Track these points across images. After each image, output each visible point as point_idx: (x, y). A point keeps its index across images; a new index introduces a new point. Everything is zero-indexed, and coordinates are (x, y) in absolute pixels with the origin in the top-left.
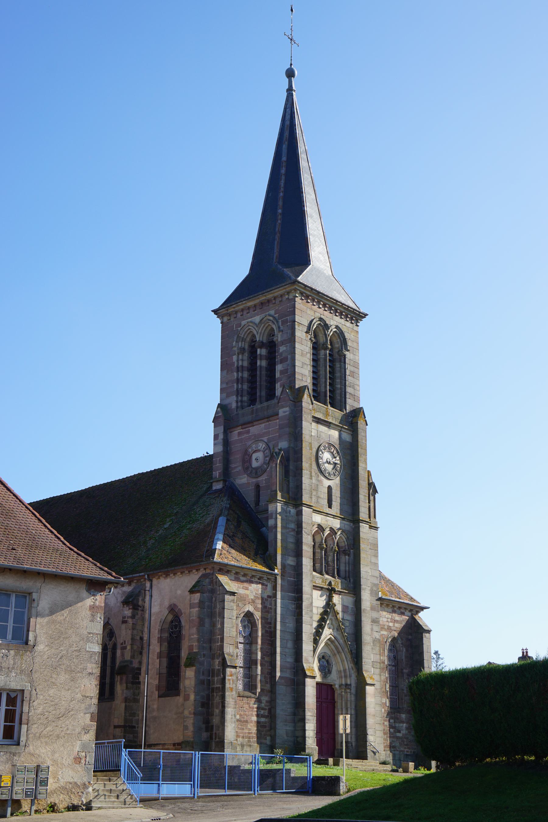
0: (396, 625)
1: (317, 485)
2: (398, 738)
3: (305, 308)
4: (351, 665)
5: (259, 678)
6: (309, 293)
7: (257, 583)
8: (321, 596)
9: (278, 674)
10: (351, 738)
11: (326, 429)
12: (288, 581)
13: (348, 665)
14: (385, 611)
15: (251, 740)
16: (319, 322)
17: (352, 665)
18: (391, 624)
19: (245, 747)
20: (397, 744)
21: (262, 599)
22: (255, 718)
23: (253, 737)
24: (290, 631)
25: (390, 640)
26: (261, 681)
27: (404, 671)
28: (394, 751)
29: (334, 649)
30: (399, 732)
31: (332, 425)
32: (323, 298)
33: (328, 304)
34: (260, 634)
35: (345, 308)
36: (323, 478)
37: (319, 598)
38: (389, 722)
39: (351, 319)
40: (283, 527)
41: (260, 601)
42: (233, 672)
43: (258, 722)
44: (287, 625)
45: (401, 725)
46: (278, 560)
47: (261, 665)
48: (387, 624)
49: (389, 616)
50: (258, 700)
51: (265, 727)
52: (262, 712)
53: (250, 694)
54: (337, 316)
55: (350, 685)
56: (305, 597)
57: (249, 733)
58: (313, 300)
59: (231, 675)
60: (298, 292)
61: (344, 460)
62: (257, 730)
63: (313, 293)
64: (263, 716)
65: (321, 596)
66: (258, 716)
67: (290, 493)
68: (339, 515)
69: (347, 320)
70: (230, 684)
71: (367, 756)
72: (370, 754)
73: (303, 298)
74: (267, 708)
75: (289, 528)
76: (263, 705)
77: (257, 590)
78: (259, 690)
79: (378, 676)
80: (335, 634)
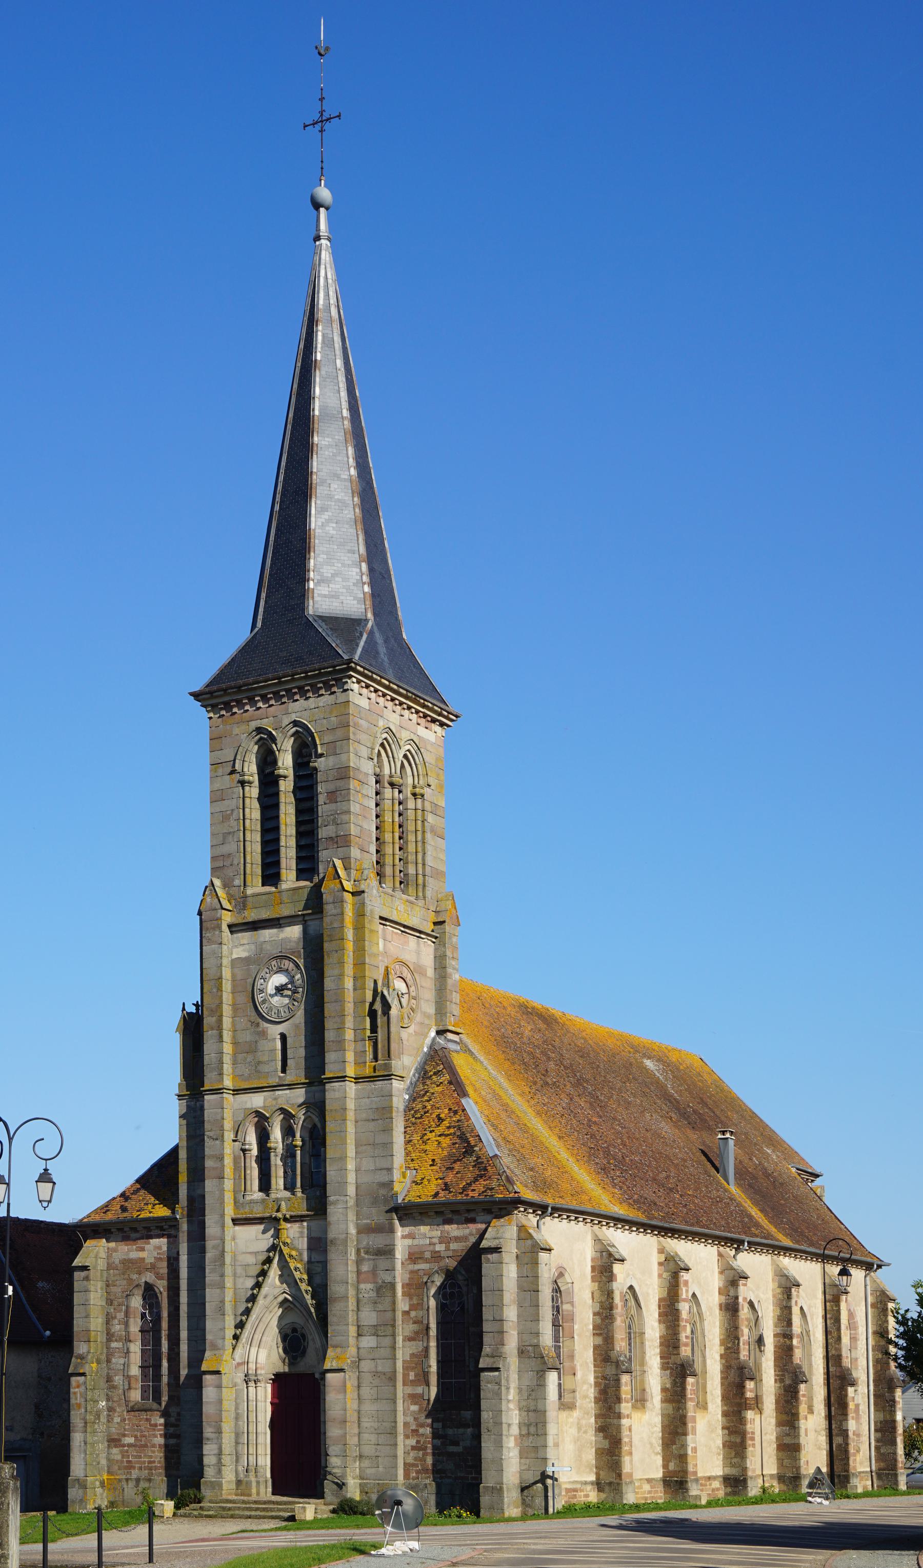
0: (453, 1246)
7: (159, 1236)
8: (264, 1232)
18: (440, 1248)
22: (160, 1440)
25: (438, 1280)
26: (169, 1384)
30: (456, 1443)
33: (269, 693)
36: (266, 1025)
37: (261, 1236)
39: (328, 687)
41: (165, 1264)
43: (166, 1446)
45: (461, 1430)
46: (180, 1194)
47: (169, 1361)
48: (431, 1248)
49: (437, 1233)
50: (165, 1414)
54: (297, 700)
56: (209, 1244)
57: (150, 1462)
58: (240, 704)
59: (78, 1387)
62: (166, 1458)
65: (264, 1232)
70: (76, 1399)
71: (324, 1493)
79: (388, 1350)
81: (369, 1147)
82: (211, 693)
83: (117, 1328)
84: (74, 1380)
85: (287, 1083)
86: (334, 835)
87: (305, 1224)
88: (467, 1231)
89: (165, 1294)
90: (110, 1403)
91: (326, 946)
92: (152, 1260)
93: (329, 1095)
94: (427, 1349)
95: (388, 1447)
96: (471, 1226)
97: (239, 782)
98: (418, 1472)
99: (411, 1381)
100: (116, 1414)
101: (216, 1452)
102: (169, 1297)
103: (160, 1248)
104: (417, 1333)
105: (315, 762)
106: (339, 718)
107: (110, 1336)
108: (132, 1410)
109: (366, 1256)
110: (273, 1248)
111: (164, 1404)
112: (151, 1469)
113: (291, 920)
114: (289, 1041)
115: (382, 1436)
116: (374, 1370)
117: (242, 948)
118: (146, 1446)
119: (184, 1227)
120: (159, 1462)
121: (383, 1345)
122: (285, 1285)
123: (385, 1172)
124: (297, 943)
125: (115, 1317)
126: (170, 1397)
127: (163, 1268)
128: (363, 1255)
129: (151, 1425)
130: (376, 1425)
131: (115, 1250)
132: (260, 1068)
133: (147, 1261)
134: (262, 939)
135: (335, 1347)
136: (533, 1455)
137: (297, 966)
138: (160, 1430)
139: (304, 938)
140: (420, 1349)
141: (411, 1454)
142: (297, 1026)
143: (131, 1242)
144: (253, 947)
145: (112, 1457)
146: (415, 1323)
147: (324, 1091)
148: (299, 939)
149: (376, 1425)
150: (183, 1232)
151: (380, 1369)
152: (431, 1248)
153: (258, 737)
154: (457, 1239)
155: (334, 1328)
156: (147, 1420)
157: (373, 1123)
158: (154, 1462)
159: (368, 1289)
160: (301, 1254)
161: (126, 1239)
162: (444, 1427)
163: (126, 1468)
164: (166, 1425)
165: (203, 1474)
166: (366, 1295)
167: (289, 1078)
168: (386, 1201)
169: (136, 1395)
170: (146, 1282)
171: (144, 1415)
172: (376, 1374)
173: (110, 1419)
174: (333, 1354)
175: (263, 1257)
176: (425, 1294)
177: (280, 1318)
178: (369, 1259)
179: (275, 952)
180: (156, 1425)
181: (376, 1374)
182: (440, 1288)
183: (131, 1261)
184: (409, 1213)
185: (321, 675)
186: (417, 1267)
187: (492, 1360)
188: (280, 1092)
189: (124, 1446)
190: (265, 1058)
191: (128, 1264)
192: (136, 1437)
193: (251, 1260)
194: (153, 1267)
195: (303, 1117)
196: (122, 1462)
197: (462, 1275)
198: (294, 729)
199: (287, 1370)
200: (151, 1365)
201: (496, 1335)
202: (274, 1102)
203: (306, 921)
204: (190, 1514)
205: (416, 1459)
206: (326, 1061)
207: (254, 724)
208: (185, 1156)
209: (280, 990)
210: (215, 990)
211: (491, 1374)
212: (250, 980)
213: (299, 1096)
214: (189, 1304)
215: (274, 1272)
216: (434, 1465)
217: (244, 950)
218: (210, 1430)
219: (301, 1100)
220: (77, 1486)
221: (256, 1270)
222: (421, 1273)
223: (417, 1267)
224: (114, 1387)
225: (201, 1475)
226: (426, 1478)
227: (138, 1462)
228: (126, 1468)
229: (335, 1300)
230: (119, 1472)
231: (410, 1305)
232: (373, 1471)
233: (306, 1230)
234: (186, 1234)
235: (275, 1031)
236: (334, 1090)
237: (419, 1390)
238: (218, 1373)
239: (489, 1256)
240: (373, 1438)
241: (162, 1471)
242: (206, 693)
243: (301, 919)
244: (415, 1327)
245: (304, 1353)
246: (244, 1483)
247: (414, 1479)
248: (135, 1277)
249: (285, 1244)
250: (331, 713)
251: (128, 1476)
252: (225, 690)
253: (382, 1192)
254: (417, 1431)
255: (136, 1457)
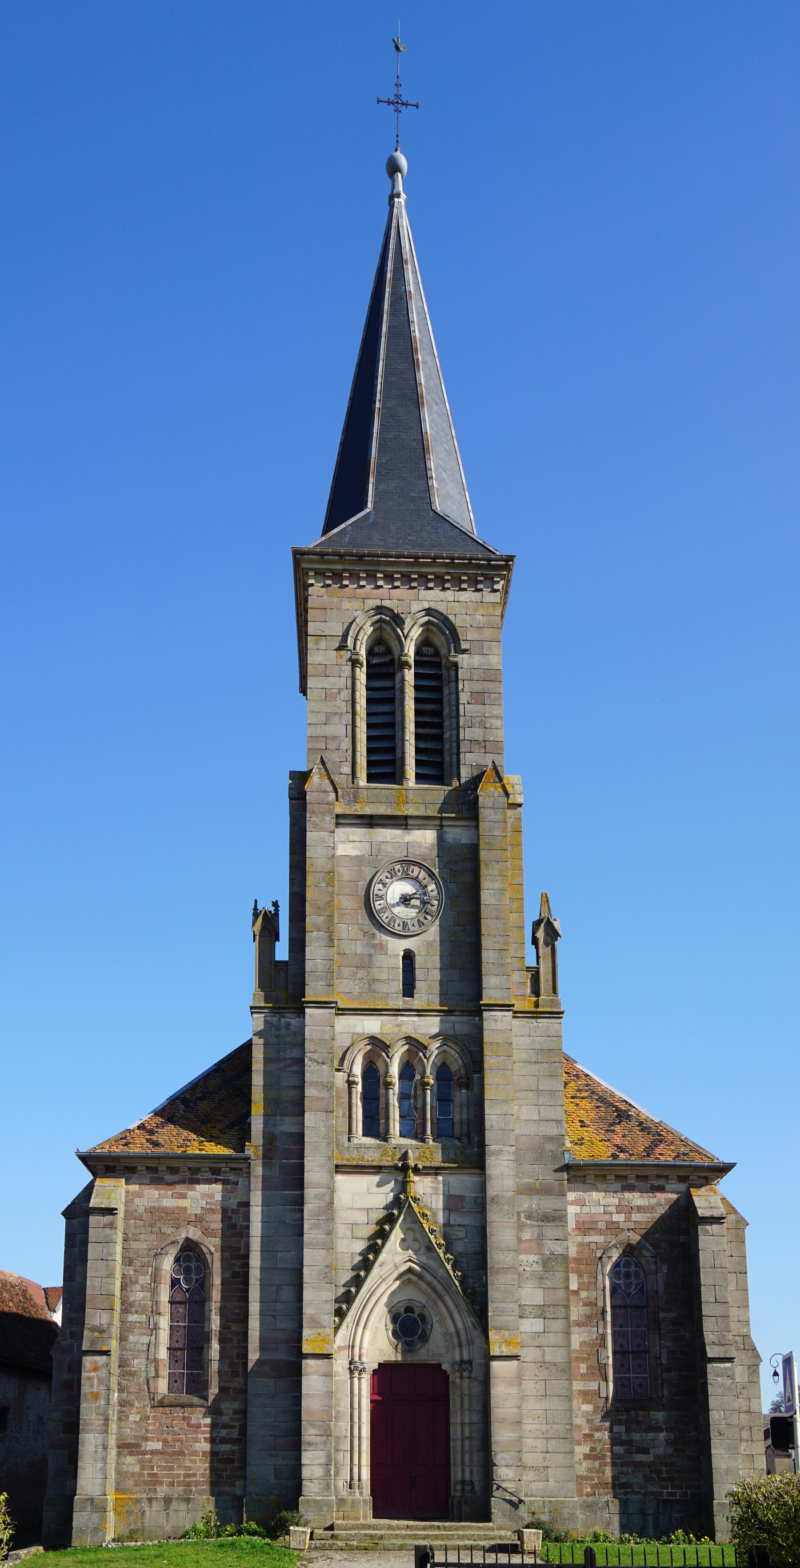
0: (636, 1217)
1: (370, 956)
2: (638, 1465)
3: (335, 600)
4: (470, 1320)
5: (215, 1366)
6: (339, 567)
7: (209, 1182)
8: (379, 1185)
9: (254, 1356)
10: (472, 1473)
11: (397, 832)
12: (282, 1166)
13: (463, 1320)
14: (597, 1190)
15: (194, 1489)
16: (426, 618)
17: (472, 1318)
18: (616, 1218)
19: (174, 1503)
20: (637, 1479)
21: (224, 1211)
22: (206, 1447)
23: (197, 1484)
24: (289, 1266)
25: (615, 1255)
26: (220, 1372)
27: (662, 1315)
28: (626, 1493)
29: (429, 1290)
30: (646, 1451)
31: (410, 822)
32: (379, 563)
33: (397, 572)
34: (217, 1280)
35: (479, 566)
36: (385, 938)
37: (375, 1189)
38: (611, 1431)
40: (267, 1060)
41: (219, 1217)
42: (101, 1363)
43: (213, 1454)
44: (280, 1255)
45: (651, 1435)
47: (221, 1341)
48: (607, 1218)
49: (613, 1200)
50: (213, 1411)
51: (232, 1461)
52: (223, 1433)
53: (196, 1400)
55: (470, 1362)
56: (309, 1193)
59: (96, 1369)
60: (311, 573)
61: (453, 886)
62: (212, 1469)
63: (351, 562)
64: (224, 1441)
65: (379, 1185)
66: (212, 1440)
67: (290, 986)
68: (263, 1005)
69: (444, 589)
70: (92, 1386)
72: (497, 1506)
73: (328, 582)
74: (237, 1424)
75: (285, 1059)
76: (225, 1419)
77: (211, 1196)
78: (214, 1390)
80: (424, 1259)
81: (531, 1094)
82: (322, 554)
83: (138, 1295)
84: (88, 1361)
85: (416, 1008)
86: (481, 739)
87: (440, 1178)
88: (654, 1201)
89: (217, 1256)
90: (124, 1396)
91: (483, 854)
92: (199, 1212)
93: (486, 1025)
94: (603, 1337)
95: (561, 1456)
96: (659, 1195)
97: (351, 659)
98: (593, 1487)
99: (582, 1375)
100: (134, 1410)
101: (322, 1460)
102: (222, 1259)
103: (211, 1196)
104: (589, 1317)
105: (456, 656)
106: (485, 618)
107: (127, 1307)
108: (161, 1404)
109: (528, 1222)
110: (397, 1203)
111: (211, 1398)
112: (188, 1485)
113: (423, 821)
114: (419, 961)
115: (553, 1441)
116: (540, 1359)
117: (351, 845)
118: (181, 1453)
119: (258, 1170)
120: (203, 1475)
121: (553, 1329)
122: (410, 1252)
123: (554, 1124)
124: (431, 850)
125: (137, 1282)
126: (222, 1389)
127: (216, 1223)
128: (523, 1219)
129: (189, 1425)
130: (544, 1428)
131: (139, 1195)
132: (377, 986)
133: (189, 1212)
134: (380, 839)
135: (499, 1329)
136: (747, 1465)
137: (431, 875)
138: (204, 1433)
139: (438, 845)
140: (594, 1336)
141: (584, 1465)
142: (429, 944)
143: (166, 1187)
144: (367, 846)
145: (125, 1468)
146: (585, 1305)
147: (481, 1019)
148: (433, 845)
149: (544, 1428)
150: (256, 1177)
151: (548, 1358)
152: (607, 1218)
153: (378, 617)
154: (639, 1209)
155: (496, 1305)
156: (184, 1418)
157: (536, 1066)
158: (194, 1475)
159: (531, 1261)
160: (434, 1215)
161: (157, 1180)
162: (628, 1431)
163: (146, 1483)
164: (213, 1426)
165: (301, 1490)
166: (527, 1269)
167: (417, 1002)
168: (554, 1158)
169: (162, 1386)
170: (187, 1239)
171: (179, 1412)
172: (543, 1364)
173: (122, 1417)
174: (496, 1337)
175: (381, 1214)
176: (599, 1271)
177: (393, 1294)
178: (531, 1226)
179: (398, 855)
180: (199, 1426)
181: (543, 1364)
182: (616, 1265)
183: (166, 1211)
184: (578, 1174)
185: (469, 565)
186: (587, 1239)
187: (722, 1349)
188: (404, 1018)
189: (145, 1453)
190: (384, 976)
191: (157, 1214)
192: (165, 1441)
193: (362, 1218)
194: (199, 1220)
195: (436, 1052)
196: (141, 1475)
197: (649, 1251)
198: (426, 618)
199: (400, 1359)
200: (190, 1346)
201: (719, 1319)
202: (396, 1030)
203: (441, 826)
204: (331, 1546)
205: (590, 1470)
206: (484, 986)
207: (373, 603)
208: (261, 1083)
209: (405, 900)
210: (323, 885)
211: (722, 1365)
212: (363, 884)
213: (431, 1026)
214: (262, 1269)
215: (397, 1235)
216: (613, 1477)
217: (354, 848)
218: (313, 1431)
219: (435, 1030)
220: (89, 1508)
221: (372, 1229)
222: (593, 1246)
223: (587, 1239)
224: (132, 1374)
225: (298, 1490)
226: (606, 1494)
227: (168, 1476)
228: (146, 1483)
229: (498, 1271)
230: (135, 1489)
231: (579, 1283)
232: (541, 1485)
233: (441, 1186)
234: (260, 1180)
235: (398, 947)
236: (495, 1021)
237: (593, 1386)
238: (328, 1356)
239: (708, 1227)
240: (540, 1444)
241: (206, 1487)
242: (316, 554)
243: (438, 822)
244: (587, 1310)
245: (424, 1338)
246: (349, 1503)
247: (588, 1495)
248: (170, 1231)
249: (416, 1200)
250: (476, 609)
251: (152, 1495)
252: (341, 556)
253: (549, 1147)
254: (591, 1436)
255: (164, 1468)
